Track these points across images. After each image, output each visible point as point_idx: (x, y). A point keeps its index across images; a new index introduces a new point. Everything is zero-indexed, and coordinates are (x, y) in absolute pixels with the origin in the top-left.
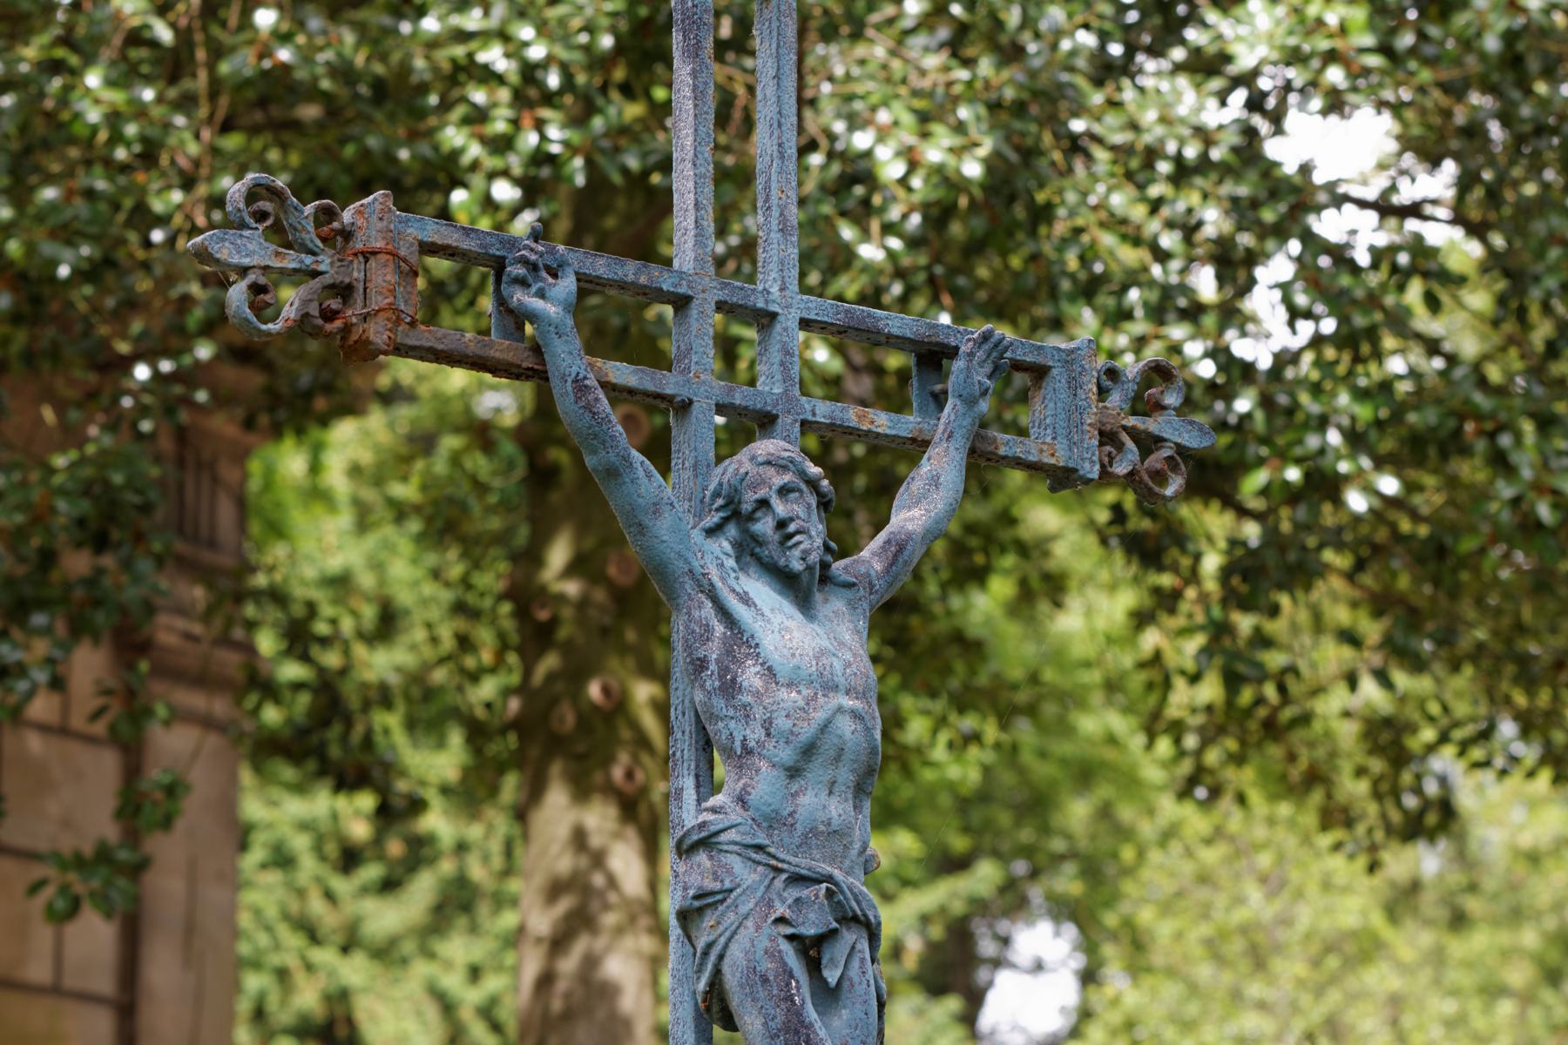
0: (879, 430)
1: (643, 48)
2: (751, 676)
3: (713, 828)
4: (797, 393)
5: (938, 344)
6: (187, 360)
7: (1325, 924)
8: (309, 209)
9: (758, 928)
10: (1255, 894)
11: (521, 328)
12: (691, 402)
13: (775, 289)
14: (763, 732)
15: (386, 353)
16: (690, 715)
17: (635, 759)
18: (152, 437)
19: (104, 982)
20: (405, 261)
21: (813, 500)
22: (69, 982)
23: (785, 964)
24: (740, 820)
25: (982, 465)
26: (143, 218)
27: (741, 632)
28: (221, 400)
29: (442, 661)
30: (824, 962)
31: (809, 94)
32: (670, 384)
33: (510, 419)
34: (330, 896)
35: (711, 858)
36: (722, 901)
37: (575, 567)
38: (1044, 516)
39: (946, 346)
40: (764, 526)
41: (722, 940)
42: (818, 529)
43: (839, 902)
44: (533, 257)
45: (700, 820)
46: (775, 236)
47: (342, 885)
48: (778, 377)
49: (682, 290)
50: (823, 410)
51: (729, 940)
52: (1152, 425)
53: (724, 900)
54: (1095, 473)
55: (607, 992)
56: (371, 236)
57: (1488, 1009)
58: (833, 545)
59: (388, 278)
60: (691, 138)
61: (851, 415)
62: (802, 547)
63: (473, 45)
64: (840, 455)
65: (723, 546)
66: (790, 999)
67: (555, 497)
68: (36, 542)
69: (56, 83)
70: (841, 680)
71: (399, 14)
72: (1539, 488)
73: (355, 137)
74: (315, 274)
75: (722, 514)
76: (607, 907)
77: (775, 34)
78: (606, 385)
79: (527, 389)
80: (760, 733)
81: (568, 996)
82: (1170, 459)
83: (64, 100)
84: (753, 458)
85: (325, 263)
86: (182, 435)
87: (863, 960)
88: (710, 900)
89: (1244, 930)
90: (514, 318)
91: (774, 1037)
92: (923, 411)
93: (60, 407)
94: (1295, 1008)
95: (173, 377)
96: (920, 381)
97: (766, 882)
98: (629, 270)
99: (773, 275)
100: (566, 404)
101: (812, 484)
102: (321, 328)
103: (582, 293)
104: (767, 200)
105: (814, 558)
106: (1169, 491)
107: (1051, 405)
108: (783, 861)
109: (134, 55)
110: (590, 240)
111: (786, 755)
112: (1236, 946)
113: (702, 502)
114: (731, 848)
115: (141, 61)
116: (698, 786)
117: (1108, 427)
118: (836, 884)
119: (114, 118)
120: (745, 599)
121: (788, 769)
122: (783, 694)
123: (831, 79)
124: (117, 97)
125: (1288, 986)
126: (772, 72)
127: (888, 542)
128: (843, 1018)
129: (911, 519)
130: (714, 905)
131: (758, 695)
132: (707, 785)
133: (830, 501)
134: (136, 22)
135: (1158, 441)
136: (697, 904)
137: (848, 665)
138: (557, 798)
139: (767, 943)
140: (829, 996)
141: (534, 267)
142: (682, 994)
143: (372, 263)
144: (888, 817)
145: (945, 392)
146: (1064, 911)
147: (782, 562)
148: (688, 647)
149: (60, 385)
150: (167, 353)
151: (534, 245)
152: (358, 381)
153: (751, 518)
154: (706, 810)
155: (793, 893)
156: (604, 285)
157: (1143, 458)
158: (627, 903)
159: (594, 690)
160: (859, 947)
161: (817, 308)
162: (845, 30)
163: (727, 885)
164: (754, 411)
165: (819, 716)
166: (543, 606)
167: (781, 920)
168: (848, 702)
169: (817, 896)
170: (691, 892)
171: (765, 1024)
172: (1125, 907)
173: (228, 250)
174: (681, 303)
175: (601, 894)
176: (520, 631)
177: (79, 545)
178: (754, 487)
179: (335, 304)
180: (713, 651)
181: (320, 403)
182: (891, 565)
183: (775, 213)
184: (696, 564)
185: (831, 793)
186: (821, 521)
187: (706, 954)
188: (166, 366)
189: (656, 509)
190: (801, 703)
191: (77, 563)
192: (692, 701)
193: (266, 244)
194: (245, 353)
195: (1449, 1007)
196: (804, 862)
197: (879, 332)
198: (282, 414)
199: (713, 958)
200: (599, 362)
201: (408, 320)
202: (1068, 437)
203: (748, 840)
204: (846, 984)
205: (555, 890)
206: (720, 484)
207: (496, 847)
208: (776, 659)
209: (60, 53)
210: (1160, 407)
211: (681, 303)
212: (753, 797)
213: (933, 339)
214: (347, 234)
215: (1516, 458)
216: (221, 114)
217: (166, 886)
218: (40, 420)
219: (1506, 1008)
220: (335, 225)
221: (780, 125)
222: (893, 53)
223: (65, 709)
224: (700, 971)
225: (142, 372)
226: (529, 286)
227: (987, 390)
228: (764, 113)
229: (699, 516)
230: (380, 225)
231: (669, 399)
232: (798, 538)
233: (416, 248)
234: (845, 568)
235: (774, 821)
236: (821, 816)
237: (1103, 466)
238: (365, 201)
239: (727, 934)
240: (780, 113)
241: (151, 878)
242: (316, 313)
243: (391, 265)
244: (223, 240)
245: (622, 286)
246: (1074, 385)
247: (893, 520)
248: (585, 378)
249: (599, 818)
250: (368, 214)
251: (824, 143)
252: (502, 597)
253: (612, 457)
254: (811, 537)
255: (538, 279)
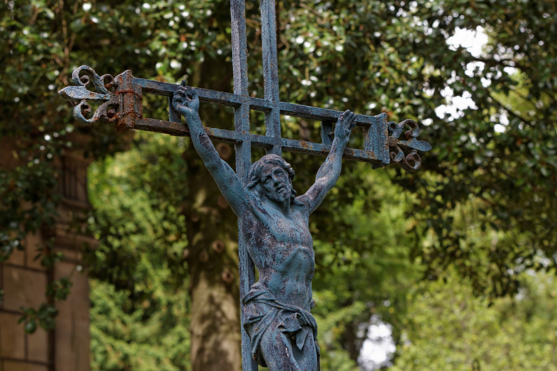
0: (310, 149)
1: (222, 14)
2: (267, 239)
3: (256, 294)
4: (280, 137)
5: (330, 117)
6: (63, 132)
7: (481, 320)
8: (102, 77)
9: (273, 329)
10: (457, 310)
11: (179, 117)
12: (242, 142)
13: (271, 100)
14: (272, 259)
15: (131, 128)
16: (246, 254)
17: (230, 270)
18: (51, 160)
19: (43, 357)
20: (137, 95)
21: (287, 175)
22: (31, 357)
23: (283, 342)
24: (265, 291)
25: (348, 162)
26: (45, 81)
27: (263, 224)
28: (76, 147)
29: (158, 238)
30: (297, 341)
31: (282, 28)
32: (234, 135)
33: (181, 150)
34: (124, 323)
35: (255, 305)
36: (260, 320)
37: (206, 203)
38: (371, 177)
39: (333, 118)
40: (270, 185)
41: (260, 334)
42: (289, 186)
43: (302, 319)
44: (183, 92)
45: (251, 291)
46: (270, 81)
47: (127, 318)
48: (273, 131)
49: (238, 101)
50: (290, 143)
51: (263, 334)
52: (409, 143)
53: (260, 320)
54: (388, 161)
55: (223, 354)
56: (124, 86)
57: (541, 349)
58: (295, 191)
59: (131, 101)
60: (238, 47)
61: (300, 144)
62: (284, 192)
63: (162, 13)
64: (299, 159)
65: (255, 193)
66: (285, 354)
67: (198, 177)
68: (10, 199)
69: (13, 35)
70: (299, 239)
71: (135, 6)
72: (542, 162)
73: (117, 50)
74: (105, 101)
75: (254, 181)
76: (222, 324)
77: (267, 8)
78: (211, 137)
79: (187, 138)
80: (271, 260)
81: (209, 356)
82: (415, 156)
83: (16, 40)
84: (265, 161)
85: (108, 96)
86: (63, 159)
87: (311, 340)
88: (255, 320)
89: (453, 322)
90: (178, 114)
91: (280, 368)
92: (326, 143)
93: (19, 151)
94: (472, 352)
95: (60, 138)
96: (324, 131)
97: (275, 313)
98: (218, 95)
99: (270, 95)
100: (197, 145)
101: (287, 169)
102: (108, 120)
103: (201, 104)
104: (267, 68)
105: (288, 196)
106: (416, 167)
107: (372, 138)
108: (281, 305)
109: (40, 23)
110: (207, 85)
111: (280, 267)
112: (450, 329)
113: (247, 177)
114: (262, 301)
115: (43, 25)
116: (250, 279)
117: (393, 145)
118: (300, 313)
119: (33, 45)
120: (264, 212)
121: (281, 272)
122: (279, 245)
123: (289, 23)
124: (35, 36)
125: (469, 343)
126: (267, 22)
127: (315, 189)
128: (305, 360)
129: (323, 181)
130: (257, 322)
131: (270, 246)
132: (253, 278)
133: (293, 175)
134: (40, 11)
135: (411, 149)
136: (251, 322)
137: (302, 234)
138: (203, 285)
139: (276, 335)
140: (299, 353)
141: (183, 95)
142: (246, 354)
143: (125, 96)
144: (319, 287)
145: (333, 135)
146: (386, 319)
147: (276, 198)
148: (244, 230)
149: (18, 143)
150: (55, 130)
151: (183, 88)
152: (126, 138)
153: (265, 182)
154: (253, 288)
155: (285, 317)
156: (209, 101)
157: (406, 155)
158: (229, 322)
159: (214, 246)
160: (309, 335)
161: (285, 105)
162: (293, 5)
163: (261, 314)
164: (265, 144)
165: (292, 253)
166: (195, 217)
167: (281, 327)
168: (303, 248)
169: (294, 317)
170: (248, 318)
171: (277, 364)
172: (410, 316)
173: (73, 92)
174: (237, 106)
175: (220, 319)
176: (187, 226)
177: (27, 200)
178: (266, 171)
179: (112, 111)
180: (253, 231)
181: (111, 147)
182: (316, 198)
183: (270, 73)
184: (246, 200)
185: (297, 280)
186: (290, 183)
187: (254, 339)
188: (56, 135)
189: (231, 180)
190: (285, 248)
191: (27, 206)
192: (246, 249)
193: (87, 91)
194: (85, 129)
195: (528, 348)
196: (288, 305)
197: (309, 114)
198: (98, 152)
199: (257, 341)
200: (208, 129)
201: (139, 116)
202: (378, 149)
203: (268, 298)
204: (305, 349)
205: (203, 318)
206: (254, 171)
207: (182, 304)
208: (276, 233)
209: (14, 23)
210: (411, 137)
211: (237, 106)
212: (270, 282)
213: (328, 116)
214: (116, 86)
215: (533, 152)
216: (72, 44)
217: (64, 322)
218: (12, 156)
219: (548, 348)
220: (112, 83)
221: (270, 41)
222: (311, 12)
223: (26, 258)
224: (253, 346)
225: (47, 138)
226: (182, 102)
227: (348, 133)
228: (265, 37)
229: (246, 182)
230: (127, 82)
231: (234, 141)
232: (282, 189)
233: (141, 90)
234: (300, 199)
235: (277, 291)
236: (294, 288)
237: (391, 159)
238: (122, 74)
239: (262, 332)
240: (270, 36)
241: (58, 319)
242: (106, 115)
243: (132, 97)
244: (71, 90)
245: (216, 101)
246: (380, 130)
247: (316, 181)
248: (204, 134)
249: (218, 292)
250: (123, 78)
251: (288, 46)
252: (179, 215)
253: (214, 162)
254: (287, 188)
255: (185, 99)
